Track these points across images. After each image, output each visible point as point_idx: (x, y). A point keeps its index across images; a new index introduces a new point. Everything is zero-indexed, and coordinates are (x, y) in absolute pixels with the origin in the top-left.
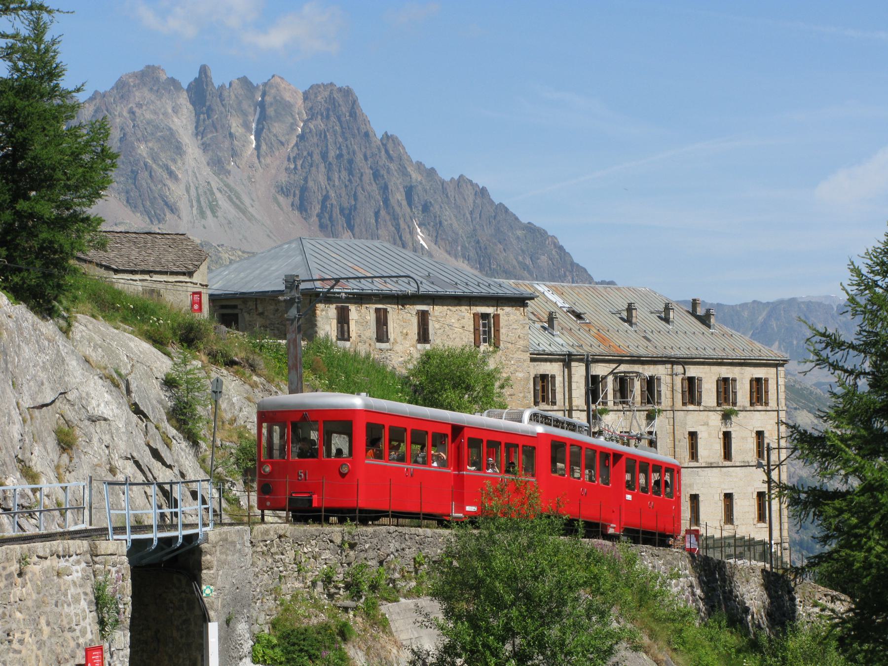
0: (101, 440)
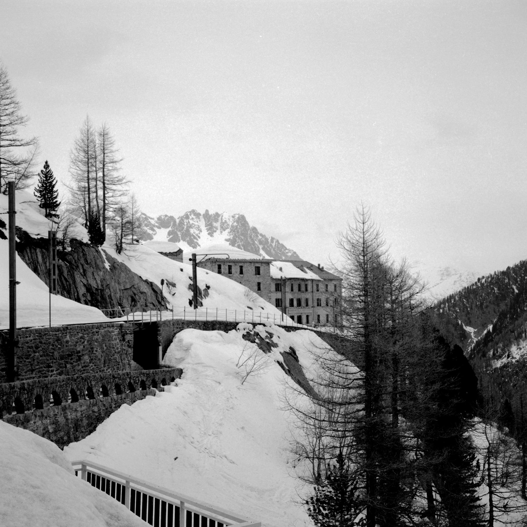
0: (143, 298)
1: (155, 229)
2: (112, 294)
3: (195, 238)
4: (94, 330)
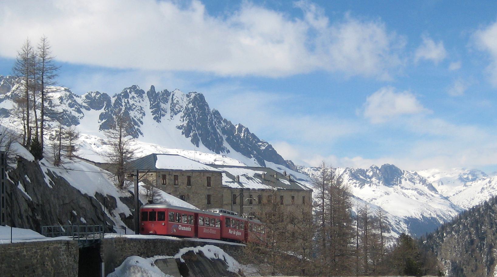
1: (83, 110)
2: (52, 210)
3: (136, 124)
4: (45, 246)
